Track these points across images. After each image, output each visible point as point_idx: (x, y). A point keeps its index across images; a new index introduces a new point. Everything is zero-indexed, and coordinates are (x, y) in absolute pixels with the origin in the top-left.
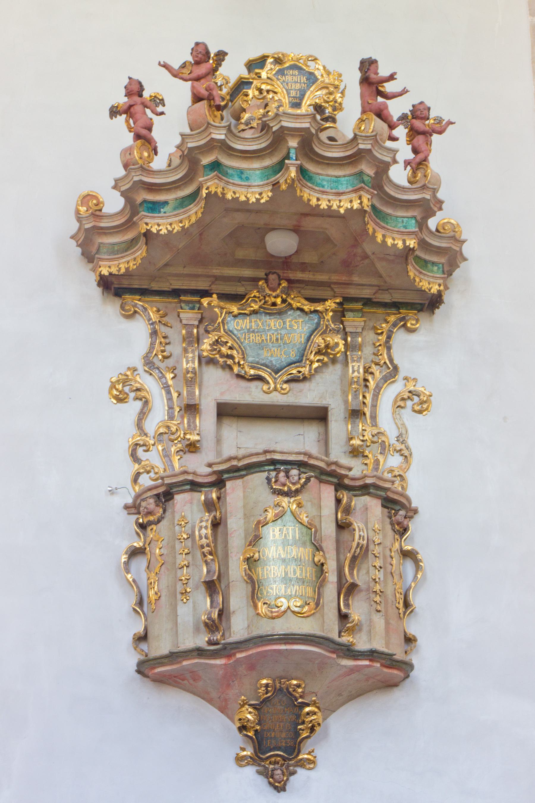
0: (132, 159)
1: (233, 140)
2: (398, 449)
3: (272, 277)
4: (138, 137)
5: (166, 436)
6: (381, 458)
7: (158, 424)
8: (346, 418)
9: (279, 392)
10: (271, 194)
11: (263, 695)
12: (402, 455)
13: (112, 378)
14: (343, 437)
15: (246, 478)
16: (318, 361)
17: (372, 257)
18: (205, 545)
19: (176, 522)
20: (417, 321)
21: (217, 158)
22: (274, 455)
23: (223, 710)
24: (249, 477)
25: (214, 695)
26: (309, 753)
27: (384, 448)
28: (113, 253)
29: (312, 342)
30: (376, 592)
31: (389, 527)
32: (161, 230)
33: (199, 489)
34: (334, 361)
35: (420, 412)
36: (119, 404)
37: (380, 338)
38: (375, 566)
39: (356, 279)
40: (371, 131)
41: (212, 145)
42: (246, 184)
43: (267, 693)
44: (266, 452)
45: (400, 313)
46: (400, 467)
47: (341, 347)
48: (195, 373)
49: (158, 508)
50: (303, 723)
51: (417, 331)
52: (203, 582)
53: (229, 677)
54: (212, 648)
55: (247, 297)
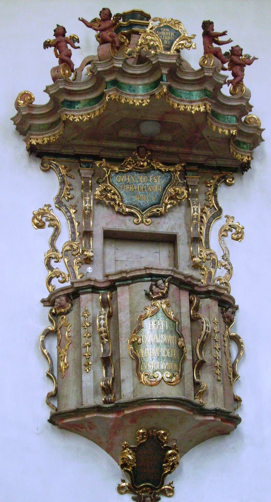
0: (58, 75)
1: (126, 67)
2: (223, 264)
3: (142, 149)
4: (62, 61)
5: (70, 252)
6: (212, 270)
7: (65, 243)
8: (189, 242)
9: (145, 224)
10: (149, 100)
11: (140, 440)
12: (226, 269)
13: (34, 212)
14: (188, 255)
15: (131, 285)
16: (170, 204)
17: (207, 138)
18: (103, 332)
19: (81, 314)
20: (233, 179)
21: (116, 77)
22: (151, 271)
23: (109, 451)
24: (134, 285)
25: (104, 439)
26: (170, 485)
27: (214, 263)
28: (39, 130)
29: (166, 192)
30: (217, 367)
31: (222, 319)
32: (75, 119)
33: (97, 291)
34: (180, 204)
35: (237, 239)
36: (38, 229)
37: (210, 189)
38: (216, 348)
39: (195, 151)
40: (211, 65)
41: (113, 70)
42: (134, 94)
43: (142, 440)
44: (146, 269)
45: (222, 173)
46: (225, 277)
47: (185, 194)
48: (91, 210)
49: (68, 303)
50: (167, 462)
51: (233, 185)
52: (100, 358)
53: (117, 427)
54: (107, 406)
55: (125, 161)
